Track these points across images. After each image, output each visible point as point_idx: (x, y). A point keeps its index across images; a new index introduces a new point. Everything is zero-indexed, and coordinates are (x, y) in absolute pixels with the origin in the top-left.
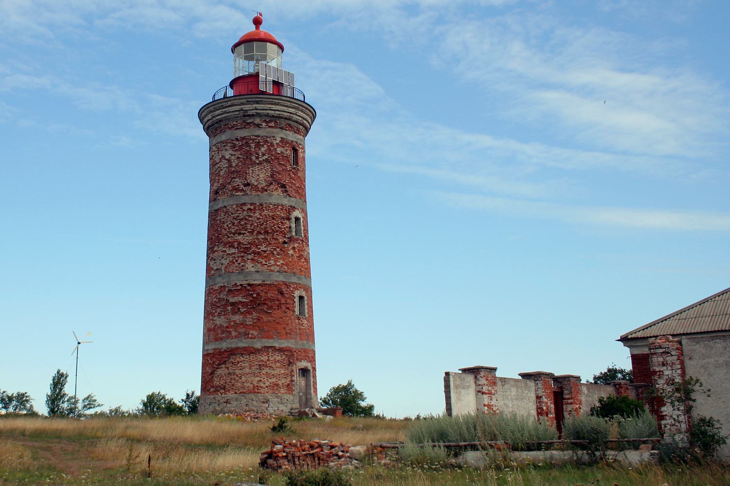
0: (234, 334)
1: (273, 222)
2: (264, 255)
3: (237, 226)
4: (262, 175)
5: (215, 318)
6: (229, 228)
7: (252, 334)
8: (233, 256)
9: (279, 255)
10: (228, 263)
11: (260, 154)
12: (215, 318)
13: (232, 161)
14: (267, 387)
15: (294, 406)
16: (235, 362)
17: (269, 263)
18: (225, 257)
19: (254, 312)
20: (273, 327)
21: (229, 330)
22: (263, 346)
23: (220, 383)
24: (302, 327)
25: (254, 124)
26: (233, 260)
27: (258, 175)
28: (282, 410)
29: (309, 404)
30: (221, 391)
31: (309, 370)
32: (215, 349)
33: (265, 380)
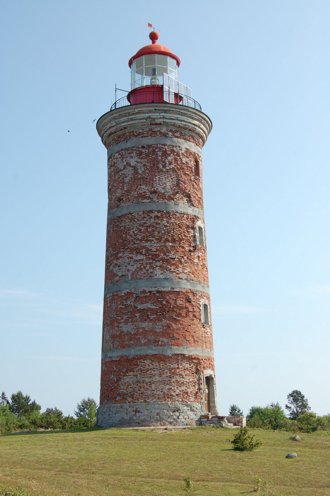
0: (143, 341)
1: (180, 230)
6: (136, 235)
7: (162, 341)
8: (141, 262)
9: (186, 263)
10: (136, 270)
14: (177, 395)
17: (177, 271)
18: (132, 263)
22: (174, 353)
23: (127, 391)
26: (141, 266)
33: (175, 388)
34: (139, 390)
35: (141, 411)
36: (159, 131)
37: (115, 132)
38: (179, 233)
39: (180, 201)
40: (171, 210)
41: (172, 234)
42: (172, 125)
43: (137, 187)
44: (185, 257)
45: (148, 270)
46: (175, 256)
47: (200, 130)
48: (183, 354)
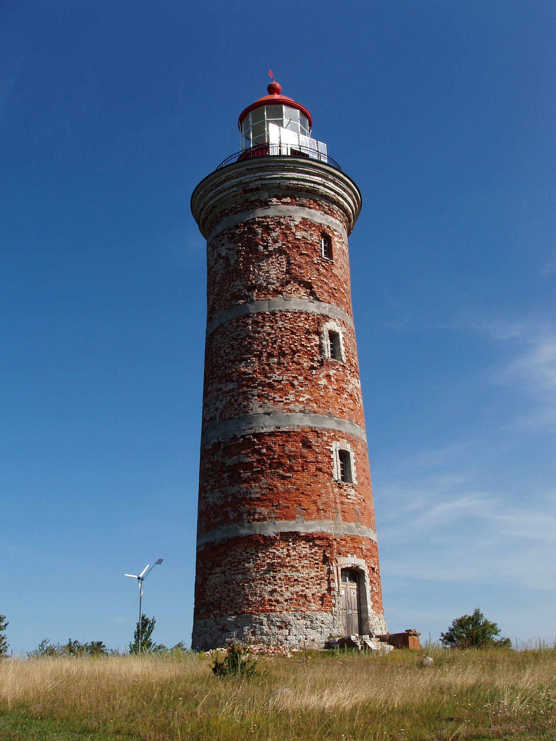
0: (232, 515)
1: (292, 338)
2: (278, 387)
3: (238, 349)
4: (273, 272)
5: (207, 495)
6: (227, 354)
7: (260, 514)
8: (232, 394)
9: (302, 387)
10: (224, 406)
11: (270, 241)
12: (207, 495)
13: (230, 257)
14: (286, 600)
15: (335, 632)
16: (235, 562)
17: (286, 399)
18: (220, 397)
19: (262, 478)
20: (295, 500)
21: (225, 510)
22: (279, 531)
23: (214, 599)
24: (347, 501)
25: (261, 202)
26: (230, 400)
27: (268, 272)
28: (313, 640)
29: (364, 628)
30: (214, 612)
31: (363, 572)
32: (206, 543)
33: (283, 589)
34: (228, 596)
35: (229, 629)
36: (258, 199)
37: (205, 217)
38: (291, 342)
39: (293, 294)
40: (278, 309)
41: (279, 345)
42: (275, 188)
43: (230, 285)
44: (299, 378)
45: (240, 404)
46: (281, 377)
47: (326, 189)
48: (295, 532)
